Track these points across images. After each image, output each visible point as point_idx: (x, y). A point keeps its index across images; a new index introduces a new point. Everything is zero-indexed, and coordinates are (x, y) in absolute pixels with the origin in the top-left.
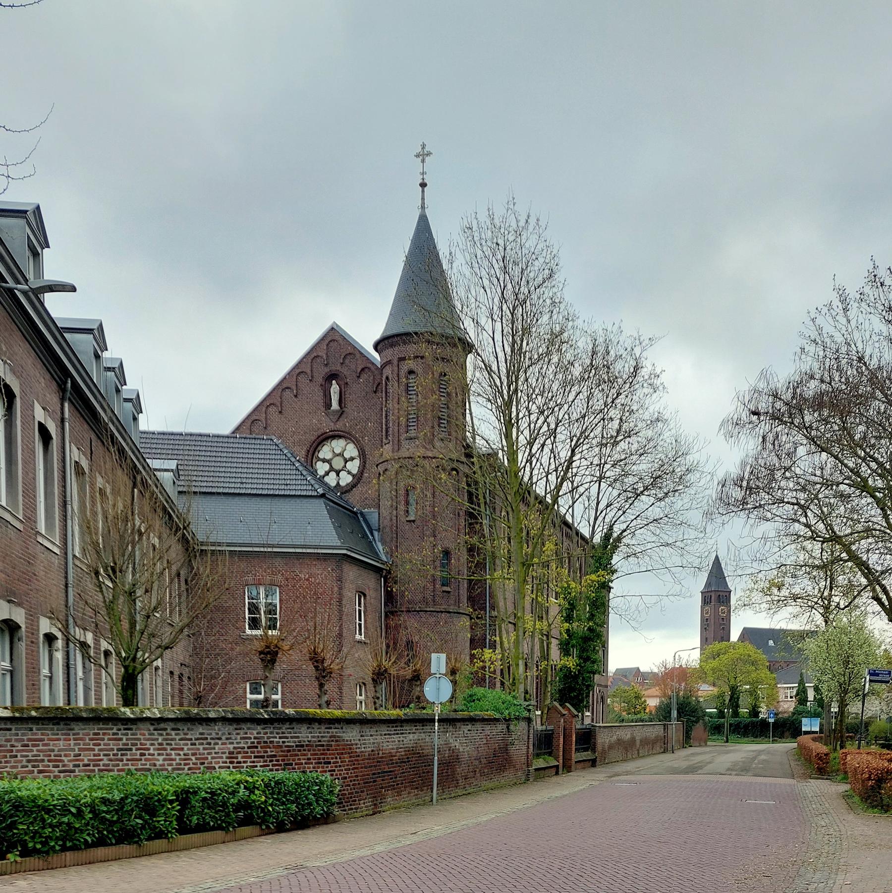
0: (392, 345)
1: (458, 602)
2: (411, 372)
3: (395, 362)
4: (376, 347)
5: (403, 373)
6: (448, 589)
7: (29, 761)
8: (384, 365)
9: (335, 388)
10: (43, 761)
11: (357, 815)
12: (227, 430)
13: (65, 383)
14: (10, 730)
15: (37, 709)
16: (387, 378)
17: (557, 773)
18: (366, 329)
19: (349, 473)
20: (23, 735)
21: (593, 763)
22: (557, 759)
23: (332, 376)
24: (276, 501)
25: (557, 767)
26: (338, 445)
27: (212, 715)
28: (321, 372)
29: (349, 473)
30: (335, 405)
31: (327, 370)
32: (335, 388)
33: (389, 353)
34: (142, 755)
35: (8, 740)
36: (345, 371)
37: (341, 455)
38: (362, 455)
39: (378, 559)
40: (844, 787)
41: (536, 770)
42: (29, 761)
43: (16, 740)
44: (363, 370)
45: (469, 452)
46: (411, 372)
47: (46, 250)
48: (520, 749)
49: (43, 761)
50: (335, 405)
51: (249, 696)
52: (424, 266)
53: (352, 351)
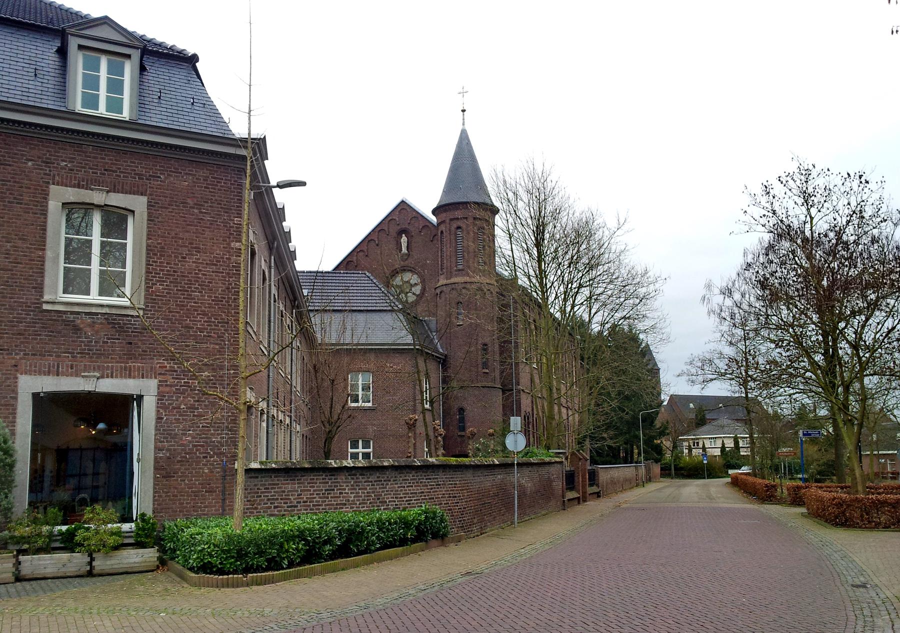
0: (445, 211)
1: (494, 380)
2: (459, 228)
3: (448, 221)
4: (435, 212)
5: (453, 229)
6: (487, 371)
7: (268, 500)
8: (439, 224)
9: (404, 239)
10: (277, 499)
11: (472, 535)
12: (329, 266)
13: (273, 244)
14: (257, 477)
15: (276, 463)
16: (442, 232)
17: (579, 503)
18: (426, 204)
19: (414, 294)
20: (266, 481)
21: (598, 495)
22: (578, 492)
23: (401, 233)
24: (369, 315)
25: (578, 498)
26: (407, 276)
27: (386, 464)
28: (393, 230)
29: (414, 294)
30: (404, 250)
31: (399, 227)
32: (404, 239)
33: (443, 216)
34: (341, 493)
35: (255, 485)
36: (411, 228)
37: (408, 282)
38: (423, 282)
39: (437, 352)
40: (803, 510)
41: (569, 500)
42: (268, 500)
43: (261, 485)
44: (423, 227)
45: (507, 280)
46: (459, 228)
47: (266, 162)
48: (559, 485)
49: (277, 499)
50: (404, 250)
51: (350, 450)
52: (464, 163)
53: (418, 216)
